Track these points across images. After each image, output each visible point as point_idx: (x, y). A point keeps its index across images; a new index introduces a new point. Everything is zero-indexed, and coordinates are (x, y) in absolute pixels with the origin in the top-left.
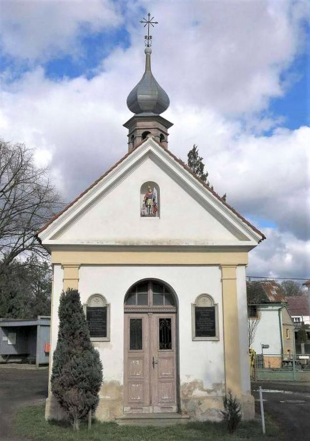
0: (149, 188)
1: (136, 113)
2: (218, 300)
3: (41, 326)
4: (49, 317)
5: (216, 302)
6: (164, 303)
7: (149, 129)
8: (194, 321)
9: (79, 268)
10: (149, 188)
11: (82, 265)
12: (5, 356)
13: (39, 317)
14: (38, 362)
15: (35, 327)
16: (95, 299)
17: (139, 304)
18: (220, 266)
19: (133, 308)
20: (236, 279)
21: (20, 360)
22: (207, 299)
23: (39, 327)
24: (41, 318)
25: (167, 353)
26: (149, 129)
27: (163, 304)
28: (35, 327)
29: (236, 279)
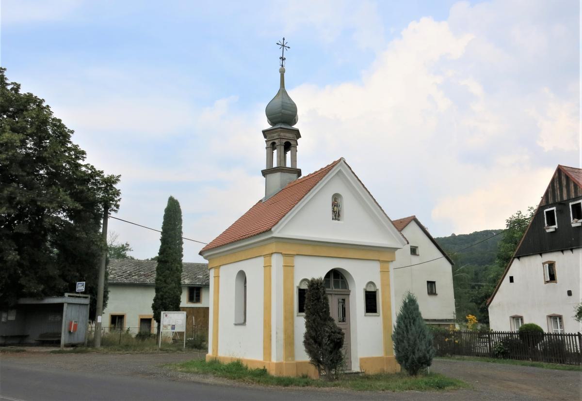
0: (336, 198)
1: (273, 126)
2: (379, 286)
3: (69, 304)
4: (348, 293)
5: (377, 288)
6: (340, 287)
7: (290, 139)
8: (365, 303)
9: (271, 256)
10: (336, 198)
11: (272, 254)
12: (6, 337)
13: (66, 295)
14: (62, 342)
15: (61, 306)
17: (342, 288)
18: (265, 256)
19: (338, 291)
20: (264, 267)
21: (14, 342)
22: (372, 285)
23: (65, 306)
24: (69, 296)
26: (290, 139)
27: (339, 288)
28: (61, 306)
29: (293, 266)
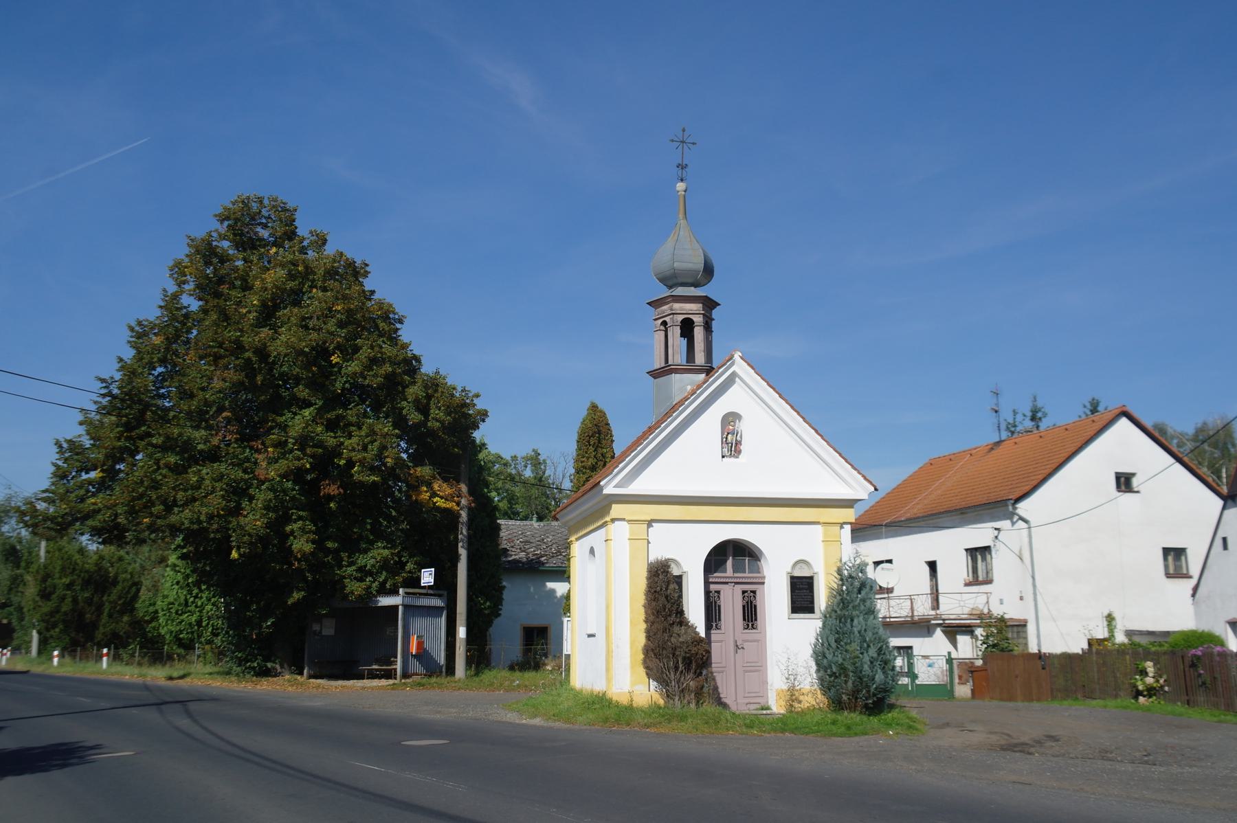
0: (730, 419)
16: (798, 566)
25: (751, 634)
